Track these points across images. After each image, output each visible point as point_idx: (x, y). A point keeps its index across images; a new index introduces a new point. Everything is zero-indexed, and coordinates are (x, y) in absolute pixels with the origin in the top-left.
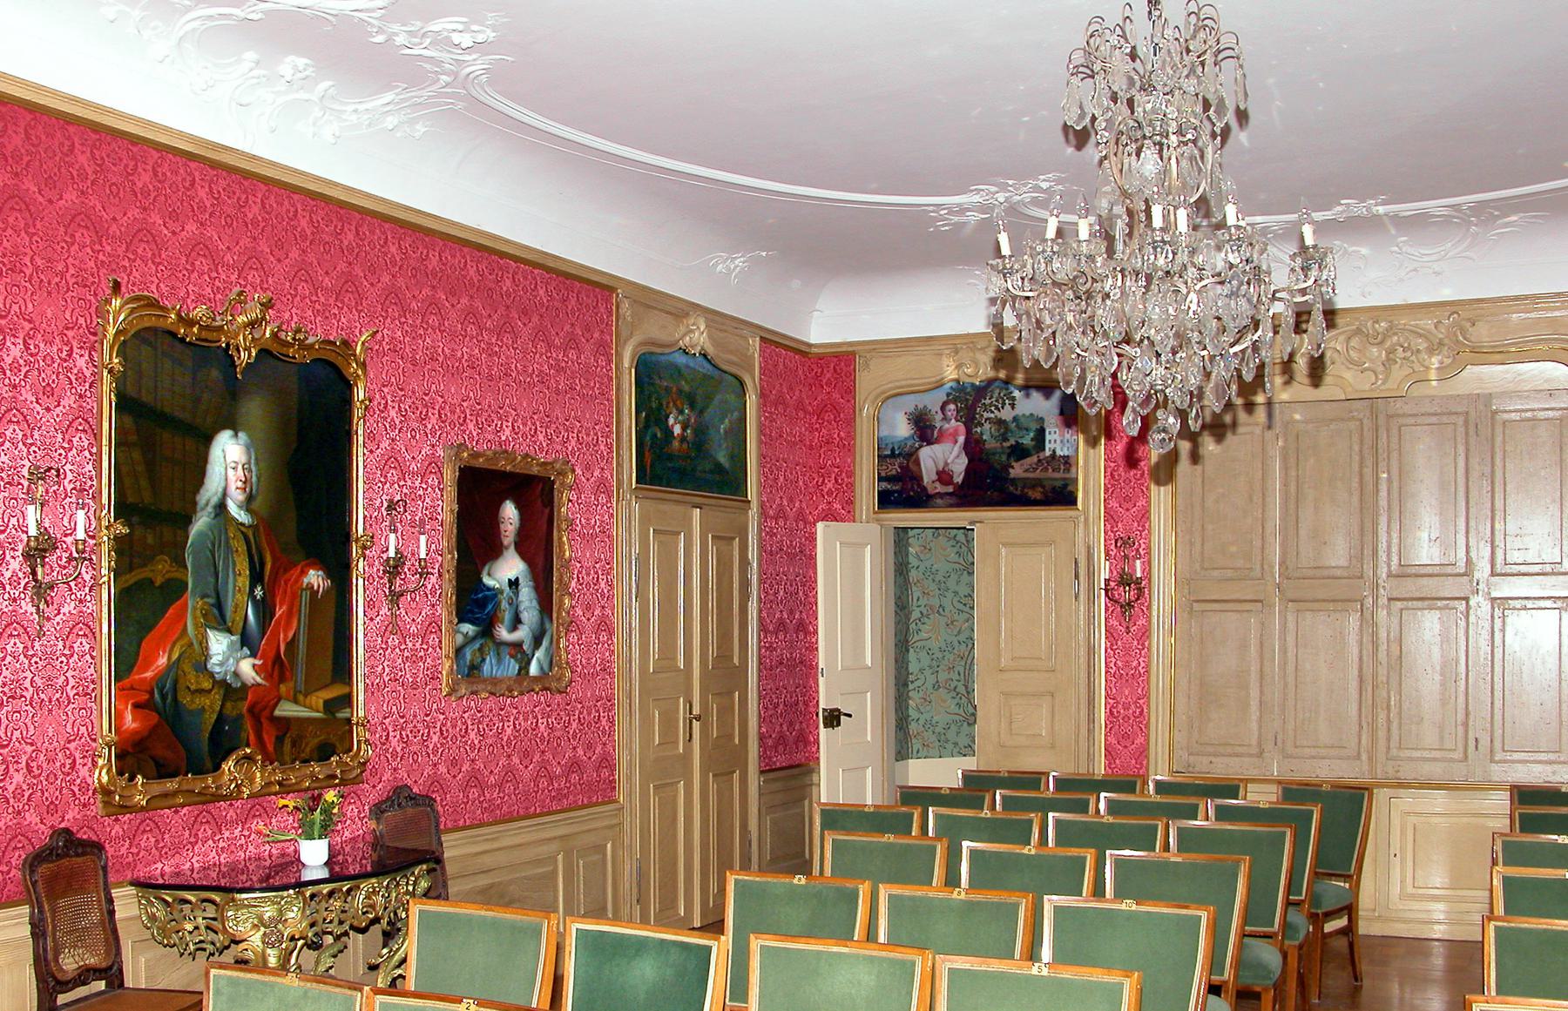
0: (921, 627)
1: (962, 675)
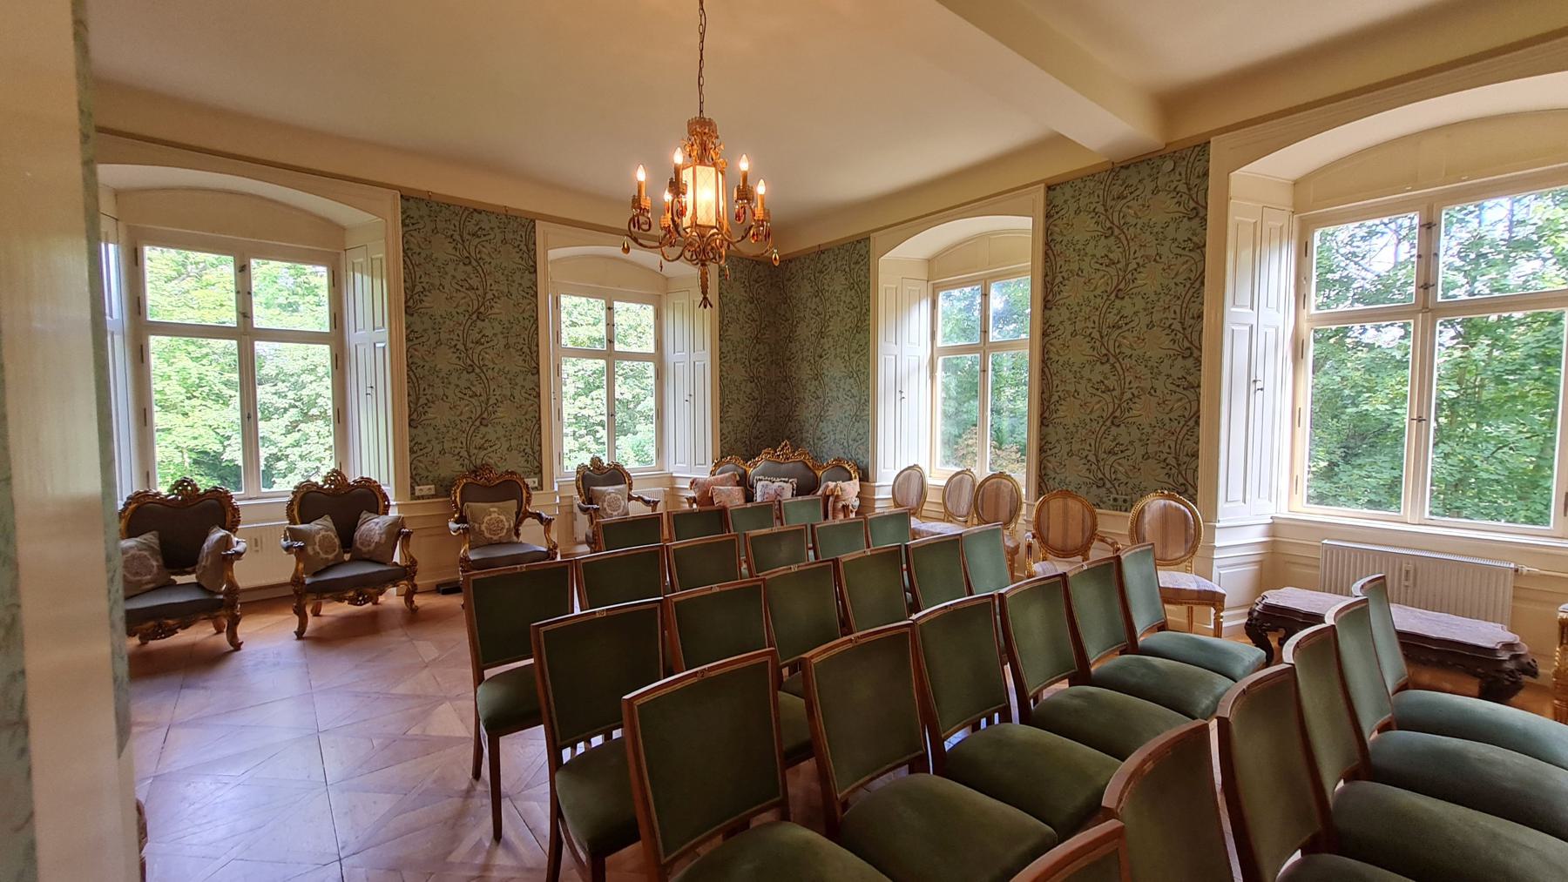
1: (464, 444)
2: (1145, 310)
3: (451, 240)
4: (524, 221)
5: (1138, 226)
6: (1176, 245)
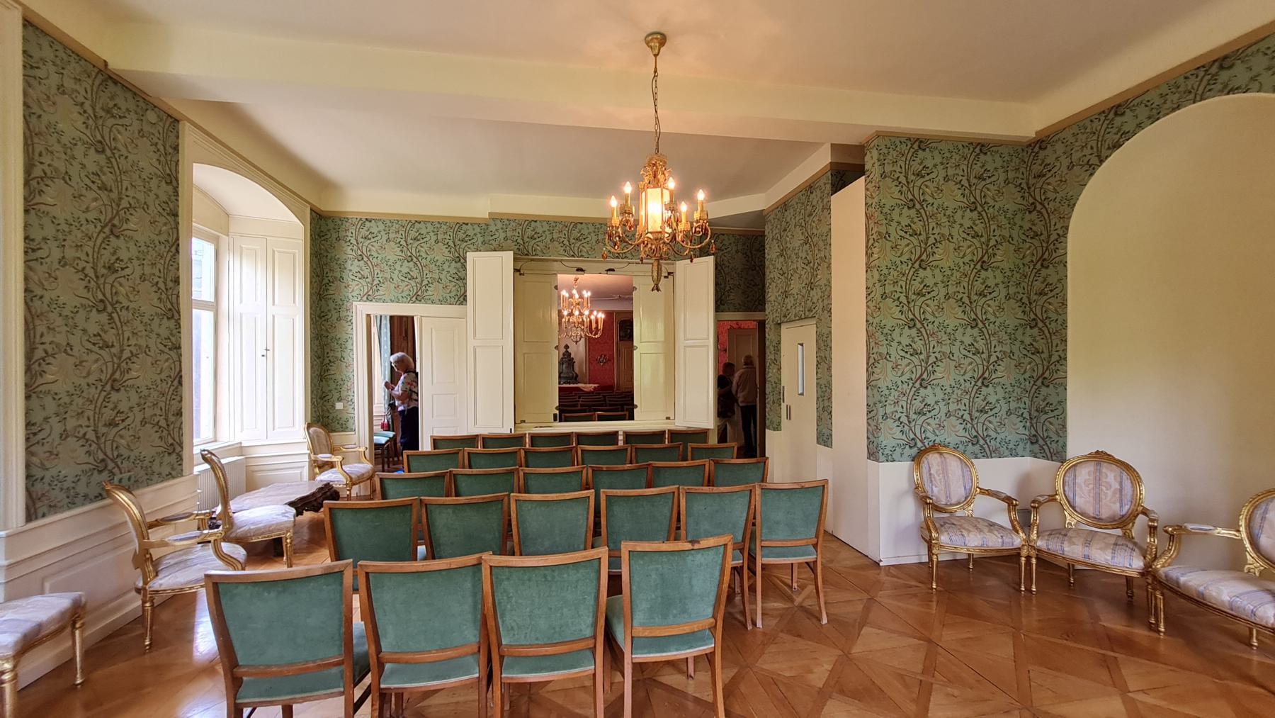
0: (936, 369)
3: (349, 244)
4: (354, 221)
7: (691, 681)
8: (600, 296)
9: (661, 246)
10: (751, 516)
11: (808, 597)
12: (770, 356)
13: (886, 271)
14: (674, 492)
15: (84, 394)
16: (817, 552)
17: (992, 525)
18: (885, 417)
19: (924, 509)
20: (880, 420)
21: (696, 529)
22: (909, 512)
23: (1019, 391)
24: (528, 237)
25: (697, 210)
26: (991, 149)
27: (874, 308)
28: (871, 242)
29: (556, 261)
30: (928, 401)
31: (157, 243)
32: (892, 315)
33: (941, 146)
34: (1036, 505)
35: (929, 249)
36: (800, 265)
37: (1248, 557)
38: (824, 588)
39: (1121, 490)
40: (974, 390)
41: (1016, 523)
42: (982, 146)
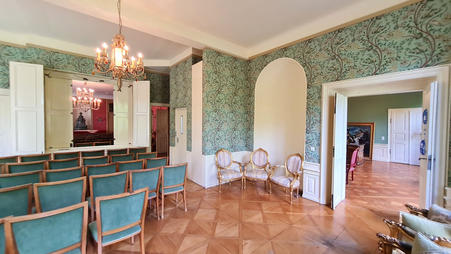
0: (313, 126)
2: (317, 92)
5: (253, 78)
6: (328, 69)
7: (133, 246)
8: (98, 92)
9: (122, 73)
10: (160, 178)
11: (181, 203)
12: (171, 120)
13: (208, 93)
14: (127, 173)
15: (229, 131)
16: (184, 187)
17: (235, 171)
18: (207, 141)
19: (218, 169)
20: (206, 142)
21: (137, 187)
22: (214, 170)
23: (243, 132)
24: (81, 64)
25: (138, 61)
26: (222, 55)
27: (204, 106)
28: (204, 83)
29: (72, 73)
30: (220, 135)
31: (229, 94)
32: (210, 108)
33: (225, 56)
34: (246, 164)
35: (237, 90)
36: (182, 88)
37: (286, 172)
38: (186, 199)
39: (264, 158)
40: (232, 132)
41: (241, 170)
42: (235, 59)
